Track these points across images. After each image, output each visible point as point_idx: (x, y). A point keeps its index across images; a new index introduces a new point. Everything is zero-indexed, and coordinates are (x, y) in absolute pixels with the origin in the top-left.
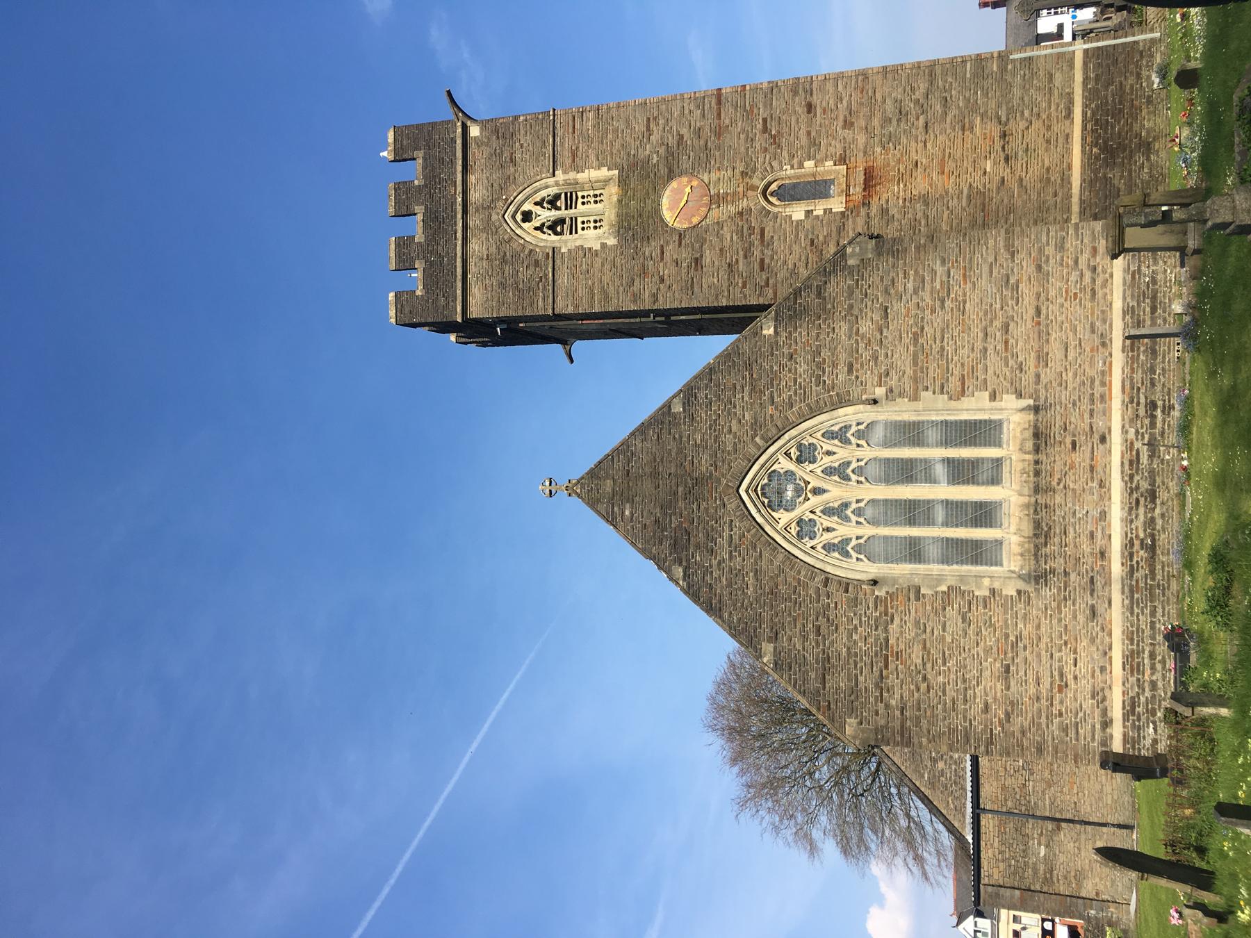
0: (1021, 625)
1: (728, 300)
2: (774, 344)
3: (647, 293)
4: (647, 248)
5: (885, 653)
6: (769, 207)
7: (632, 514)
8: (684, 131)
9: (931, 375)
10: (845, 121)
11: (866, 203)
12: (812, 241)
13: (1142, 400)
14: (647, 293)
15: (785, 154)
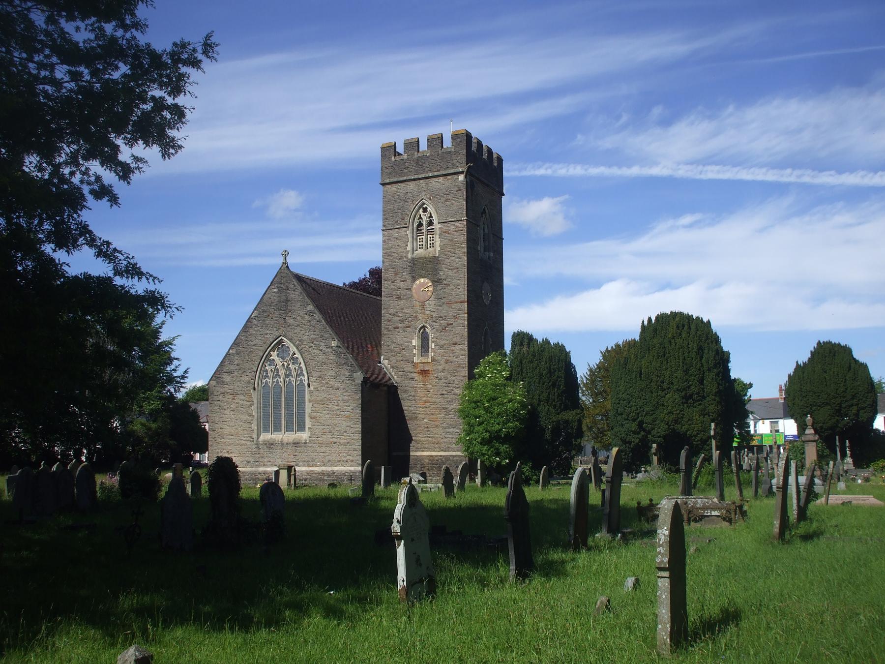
0: (244, 439)
1: (384, 314)
3: (388, 275)
5: (234, 395)
6: (418, 329)
7: (274, 292)
8: (451, 286)
9: (317, 406)
10: (448, 360)
12: (404, 349)
13: (307, 477)
14: (388, 275)
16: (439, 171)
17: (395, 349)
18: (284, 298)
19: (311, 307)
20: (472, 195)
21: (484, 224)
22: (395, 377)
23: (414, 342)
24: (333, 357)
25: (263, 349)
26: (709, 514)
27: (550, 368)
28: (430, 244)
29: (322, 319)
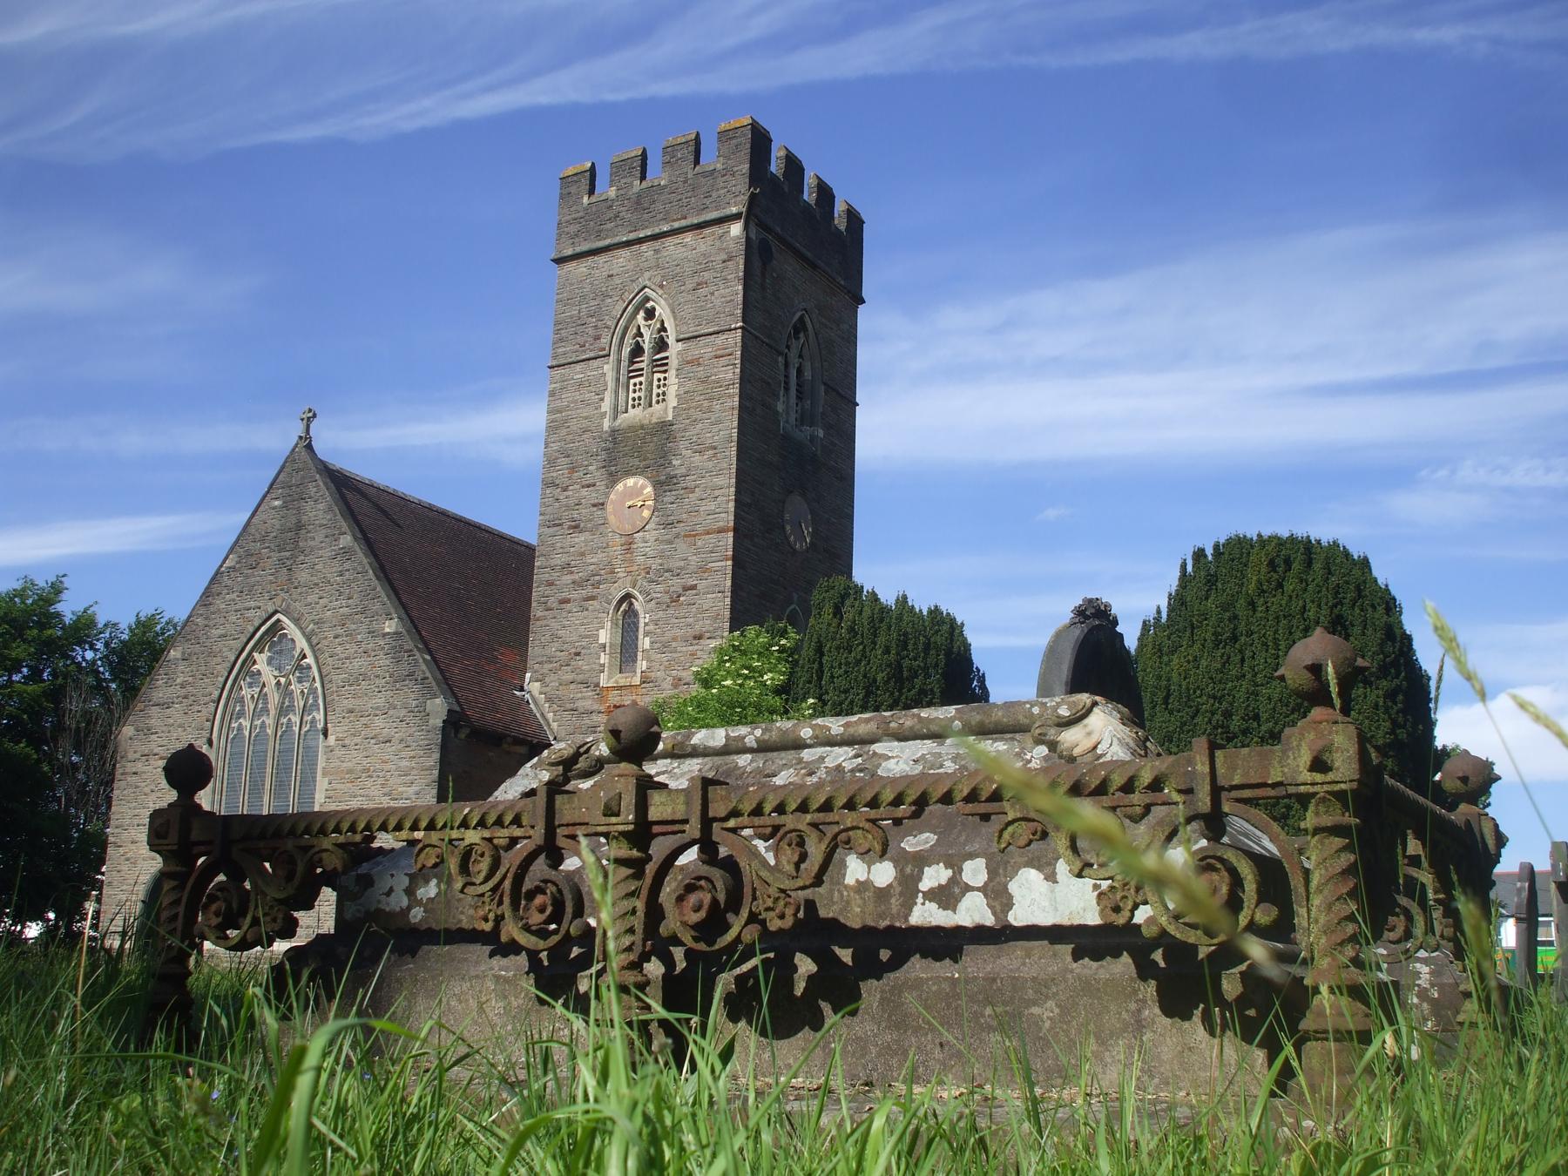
1: (539, 568)
3: (555, 474)
4: (595, 467)
9: (339, 786)
10: (680, 680)
12: (578, 654)
14: (555, 474)
16: (685, 218)
17: (558, 653)
18: (294, 520)
19: (346, 540)
20: (763, 275)
21: (800, 356)
22: (555, 725)
23: (604, 636)
24: (384, 661)
25: (238, 645)
26: (973, 911)
27: (900, 666)
28: (658, 395)
29: (367, 567)
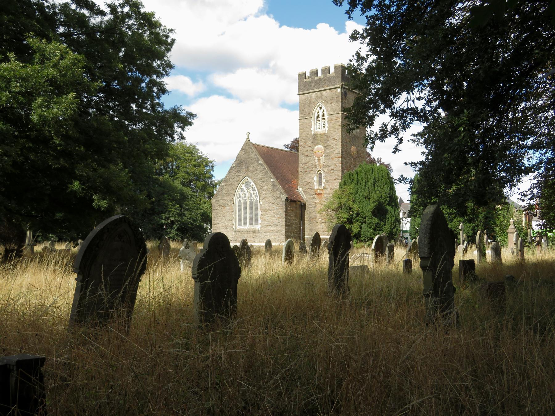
2: (269, 181)
5: (224, 206)
11: (316, 194)
15: (327, 175)
